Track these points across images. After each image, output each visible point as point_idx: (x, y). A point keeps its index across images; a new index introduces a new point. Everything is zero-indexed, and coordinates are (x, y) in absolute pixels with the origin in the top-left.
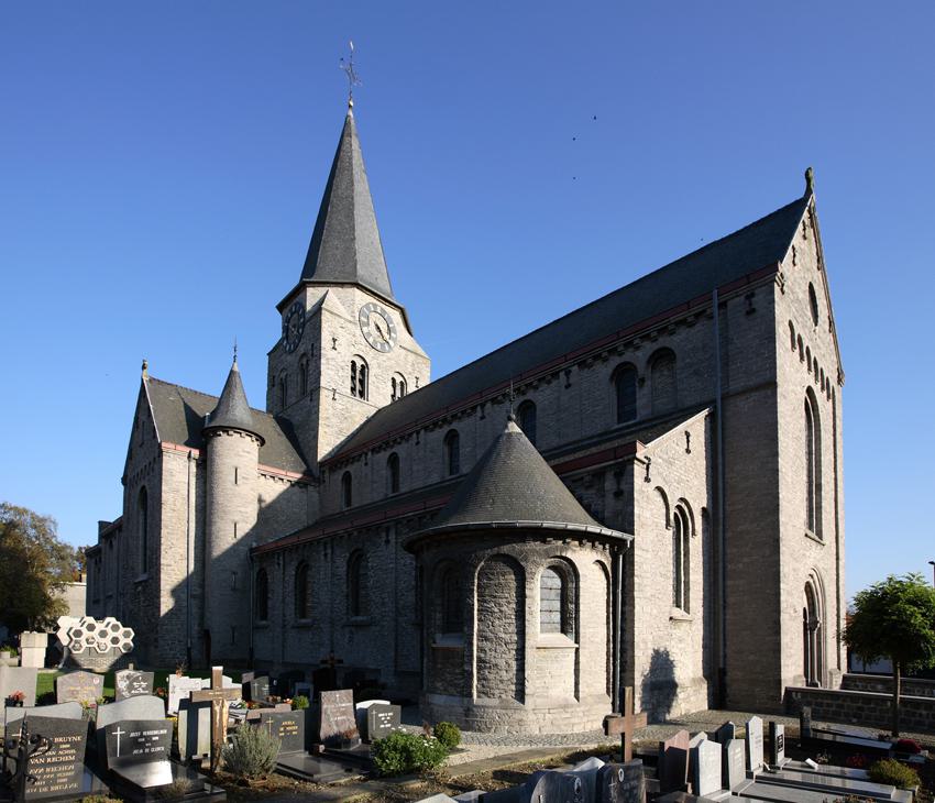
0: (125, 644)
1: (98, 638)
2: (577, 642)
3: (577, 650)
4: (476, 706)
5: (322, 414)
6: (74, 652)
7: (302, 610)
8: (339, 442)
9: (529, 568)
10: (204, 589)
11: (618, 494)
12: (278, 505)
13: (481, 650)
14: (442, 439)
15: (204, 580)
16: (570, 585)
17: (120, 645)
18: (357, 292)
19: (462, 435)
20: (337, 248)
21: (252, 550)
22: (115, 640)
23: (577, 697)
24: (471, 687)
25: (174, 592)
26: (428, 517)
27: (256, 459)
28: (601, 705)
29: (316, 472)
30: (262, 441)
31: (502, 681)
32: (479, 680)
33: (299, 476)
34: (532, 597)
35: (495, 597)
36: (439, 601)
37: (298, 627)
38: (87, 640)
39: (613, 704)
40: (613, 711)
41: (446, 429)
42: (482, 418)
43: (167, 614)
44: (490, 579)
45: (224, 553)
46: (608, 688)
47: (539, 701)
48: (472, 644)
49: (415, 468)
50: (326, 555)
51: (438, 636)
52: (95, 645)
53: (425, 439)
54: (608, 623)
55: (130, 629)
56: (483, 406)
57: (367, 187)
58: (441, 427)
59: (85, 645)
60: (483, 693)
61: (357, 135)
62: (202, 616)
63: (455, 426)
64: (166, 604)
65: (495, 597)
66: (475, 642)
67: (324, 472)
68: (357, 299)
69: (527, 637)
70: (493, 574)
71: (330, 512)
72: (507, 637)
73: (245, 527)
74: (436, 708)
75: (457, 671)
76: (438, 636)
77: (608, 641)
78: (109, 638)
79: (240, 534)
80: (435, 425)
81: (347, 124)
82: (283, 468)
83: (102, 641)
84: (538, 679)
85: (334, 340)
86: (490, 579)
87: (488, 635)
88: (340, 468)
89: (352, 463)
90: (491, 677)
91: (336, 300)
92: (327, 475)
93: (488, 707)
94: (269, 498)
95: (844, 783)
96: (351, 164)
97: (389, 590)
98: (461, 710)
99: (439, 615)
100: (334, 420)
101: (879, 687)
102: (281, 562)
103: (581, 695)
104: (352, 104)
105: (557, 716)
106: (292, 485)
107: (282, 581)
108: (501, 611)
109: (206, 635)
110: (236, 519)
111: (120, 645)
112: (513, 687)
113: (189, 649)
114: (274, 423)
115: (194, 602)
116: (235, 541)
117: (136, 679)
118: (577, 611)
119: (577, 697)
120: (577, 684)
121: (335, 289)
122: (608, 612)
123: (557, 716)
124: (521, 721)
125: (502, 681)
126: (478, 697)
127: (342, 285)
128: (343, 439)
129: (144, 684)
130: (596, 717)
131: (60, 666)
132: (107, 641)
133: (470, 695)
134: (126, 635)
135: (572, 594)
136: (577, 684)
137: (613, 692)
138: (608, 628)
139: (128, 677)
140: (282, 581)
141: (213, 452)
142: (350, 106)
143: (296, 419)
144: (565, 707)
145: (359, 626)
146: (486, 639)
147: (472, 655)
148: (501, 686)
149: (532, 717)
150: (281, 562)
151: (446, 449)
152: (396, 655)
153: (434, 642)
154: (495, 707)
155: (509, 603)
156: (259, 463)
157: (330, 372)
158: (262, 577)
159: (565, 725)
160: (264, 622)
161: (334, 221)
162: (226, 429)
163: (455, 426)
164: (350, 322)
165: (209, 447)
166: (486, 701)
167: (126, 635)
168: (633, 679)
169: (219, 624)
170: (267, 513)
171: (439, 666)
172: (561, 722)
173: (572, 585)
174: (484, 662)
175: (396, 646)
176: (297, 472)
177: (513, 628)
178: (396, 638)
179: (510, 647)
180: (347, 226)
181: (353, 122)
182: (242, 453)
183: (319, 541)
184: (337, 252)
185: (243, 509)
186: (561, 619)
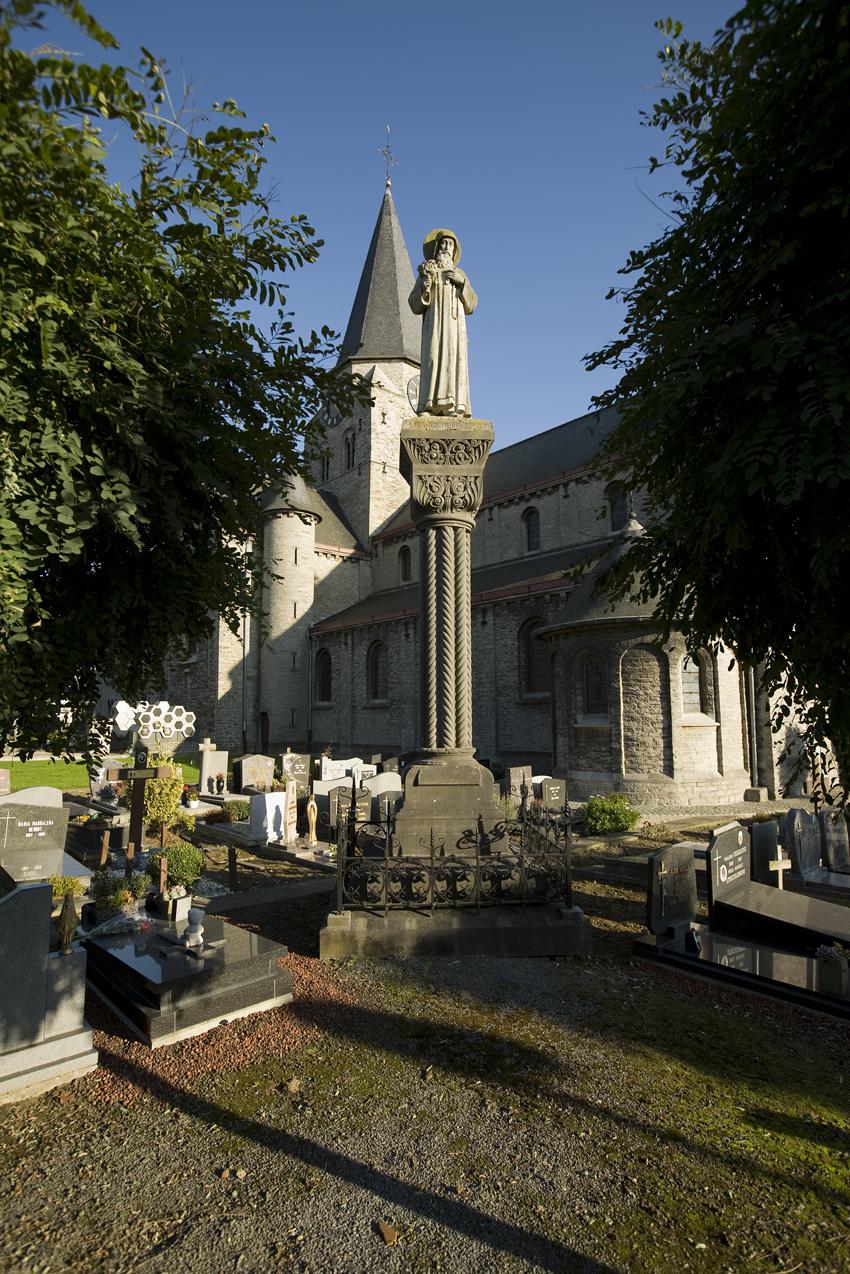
0: (188, 728)
1: (163, 723)
2: (718, 719)
3: (718, 728)
4: (626, 781)
5: (373, 488)
6: (142, 737)
7: (375, 689)
8: (389, 514)
9: (672, 656)
10: (259, 670)
11: (366, 442)
12: (330, 582)
13: (628, 729)
14: (519, 515)
15: (259, 662)
16: (708, 669)
17: (183, 729)
18: (405, 366)
19: (542, 513)
20: (381, 324)
21: (311, 630)
22: (179, 725)
23: (721, 771)
24: (620, 763)
25: (232, 674)
26: (532, 600)
27: (313, 538)
28: (741, 780)
29: (367, 546)
30: (319, 519)
31: (650, 758)
32: (627, 756)
33: (351, 551)
34: (676, 681)
35: (640, 681)
36: (579, 685)
37: (371, 708)
38: (154, 725)
39: (752, 778)
40: (752, 785)
41: (524, 506)
42: (566, 497)
43: (224, 696)
44: (634, 665)
45: (283, 634)
46: (745, 764)
47: (687, 775)
48: (619, 724)
49: (488, 543)
50: (407, 635)
51: (580, 717)
52: (161, 730)
53: (499, 516)
54: (742, 702)
55: (192, 713)
56: (566, 485)
57: (409, 262)
58: (517, 504)
59: (152, 730)
60: (632, 768)
61: (396, 213)
62: (258, 699)
63: (533, 503)
64: (224, 686)
65: (640, 681)
66: (622, 722)
67: (376, 546)
68: (405, 372)
69: (673, 717)
70: (637, 661)
71: (385, 587)
72: (653, 717)
73: (305, 606)
74: (580, 783)
75: (603, 749)
76: (580, 717)
77: (743, 719)
78: (173, 722)
79: (300, 614)
80: (511, 502)
81: (385, 202)
82: (335, 545)
83: (167, 725)
84: (685, 754)
85: (384, 415)
86: (634, 665)
87: (637, 714)
88: (397, 542)
89: (411, 537)
90: (639, 753)
91: (381, 371)
92: (380, 548)
93: (638, 782)
94: (323, 574)
95: (767, 964)
96: (391, 241)
97: (488, 670)
98: (610, 785)
99: (579, 698)
100: (384, 493)
101: (221, 784)
102: (349, 642)
103: (724, 769)
104: (389, 183)
105: (704, 789)
106: (344, 561)
107: (350, 662)
108: (646, 694)
109: (263, 718)
110: (296, 598)
111: (183, 729)
112: (661, 763)
113: (244, 733)
114: (319, 498)
115: (250, 684)
116: (295, 621)
117: (297, 762)
118: (716, 692)
119: (721, 771)
120: (720, 760)
121: (382, 364)
122: (741, 692)
123: (704, 789)
124: (671, 793)
125: (650, 758)
126: (627, 772)
127: (389, 360)
128: (394, 511)
129: (303, 766)
130: (738, 791)
131: (131, 751)
132: (171, 725)
133: (619, 771)
134: (188, 719)
135: (710, 677)
136: (720, 760)
137: (751, 767)
138: (742, 708)
139: (291, 760)
140: (350, 662)
141: (271, 533)
142: (388, 185)
143: (341, 492)
144: (711, 781)
145: (381, 708)
146: (633, 719)
147: (620, 734)
148: (649, 762)
149: (681, 790)
150: (349, 642)
151: (524, 525)
152: (497, 735)
153: (576, 723)
154: (645, 782)
155: (654, 686)
156: (316, 541)
157: (380, 446)
158: (324, 657)
159: (712, 797)
160: (325, 704)
161: (377, 298)
162: (286, 512)
163: (533, 503)
164: (399, 396)
165: (266, 529)
166: (634, 776)
167: (188, 719)
168: (772, 755)
169: (278, 708)
170: (322, 589)
171: (582, 744)
172: (708, 794)
173: (709, 669)
174: (631, 740)
175: (496, 725)
176: (348, 547)
177: (658, 709)
178: (497, 720)
179: (657, 726)
180: (391, 301)
181: (391, 201)
182: (301, 534)
183: (398, 622)
184: (382, 328)
185: (302, 589)
186: (701, 699)
